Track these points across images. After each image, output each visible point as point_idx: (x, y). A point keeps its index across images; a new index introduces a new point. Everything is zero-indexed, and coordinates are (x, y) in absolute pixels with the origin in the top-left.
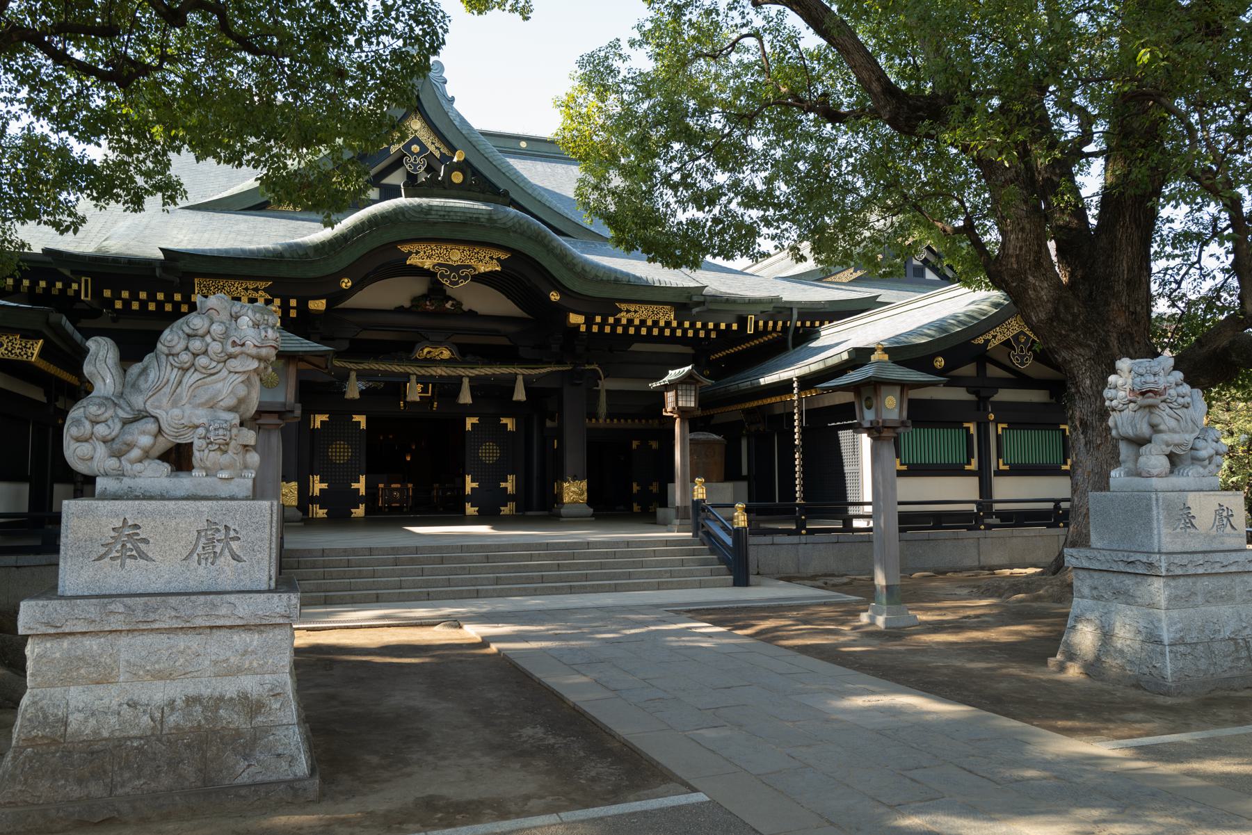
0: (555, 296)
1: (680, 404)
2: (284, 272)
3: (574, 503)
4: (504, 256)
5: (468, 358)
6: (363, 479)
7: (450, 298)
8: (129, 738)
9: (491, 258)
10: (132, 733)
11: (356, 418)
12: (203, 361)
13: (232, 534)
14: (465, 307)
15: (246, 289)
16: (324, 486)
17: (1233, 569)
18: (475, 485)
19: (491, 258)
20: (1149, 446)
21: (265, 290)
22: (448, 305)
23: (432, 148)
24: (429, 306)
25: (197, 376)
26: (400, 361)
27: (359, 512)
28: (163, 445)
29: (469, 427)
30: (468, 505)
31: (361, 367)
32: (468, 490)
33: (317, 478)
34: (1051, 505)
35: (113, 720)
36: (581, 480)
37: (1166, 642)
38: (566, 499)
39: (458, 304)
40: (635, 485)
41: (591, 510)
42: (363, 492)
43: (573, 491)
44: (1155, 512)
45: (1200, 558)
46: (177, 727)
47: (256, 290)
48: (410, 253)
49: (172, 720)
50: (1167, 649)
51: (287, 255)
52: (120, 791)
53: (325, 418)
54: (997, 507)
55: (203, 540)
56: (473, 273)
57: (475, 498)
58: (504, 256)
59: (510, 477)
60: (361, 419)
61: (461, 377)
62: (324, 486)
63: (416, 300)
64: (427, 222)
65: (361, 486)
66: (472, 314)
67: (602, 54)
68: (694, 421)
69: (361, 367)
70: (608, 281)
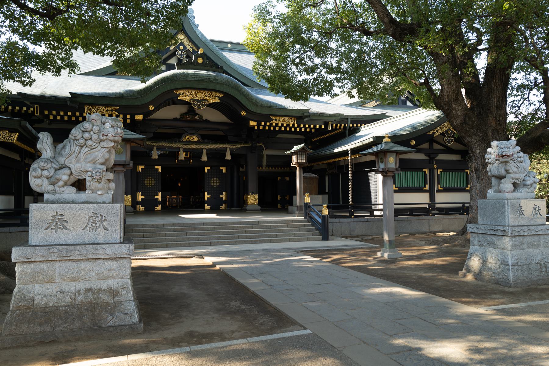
0: (243, 113)
1: (299, 161)
2: (124, 103)
3: (252, 204)
4: (221, 96)
5: (206, 141)
6: (160, 194)
7: (197, 114)
8: (61, 306)
9: (215, 96)
10: (62, 304)
11: (157, 167)
12: (89, 143)
13: (104, 218)
14: (204, 118)
15: (108, 110)
16: (143, 197)
17: (540, 233)
18: (209, 196)
19: (215, 96)
20: (505, 179)
21: (116, 111)
22: (196, 117)
23: (189, 47)
24: (188, 118)
25: (87, 149)
26: (176, 142)
27: (159, 208)
28: (73, 179)
29: (206, 171)
30: (206, 205)
31: (158, 144)
32: (206, 199)
33: (140, 193)
34: (461, 205)
35: (54, 298)
36: (255, 194)
37: (510, 265)
38: (249, 203)
39: (201, 117)
40: (279, 196)
41: (260, 207)
42: (160, 199)
43: (252, 199)
44: (506, 208)
45: (526, 228)
46: (82, 302)
47: (112, 111)
48: (180, 94)
49: (79, 298)
50: (511, 267)
51: (125, 95)
52: (58, 329)
53: (143, 167)
54: (437, 206)
55: (91, 221)
56: (207, 103)
57: (209, 202)
58: (221, 96)
59: (224, 193)
60: (159, 168)
61: (202, 149)
62: (143, 197)
63: (182, 115)
64: (187, 81)
65: (159, 197)
66: (207, 121)
67: (264, 5)
68: (304, 168)
69: (158, 144)
70: (267, 107)
